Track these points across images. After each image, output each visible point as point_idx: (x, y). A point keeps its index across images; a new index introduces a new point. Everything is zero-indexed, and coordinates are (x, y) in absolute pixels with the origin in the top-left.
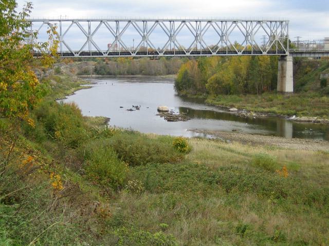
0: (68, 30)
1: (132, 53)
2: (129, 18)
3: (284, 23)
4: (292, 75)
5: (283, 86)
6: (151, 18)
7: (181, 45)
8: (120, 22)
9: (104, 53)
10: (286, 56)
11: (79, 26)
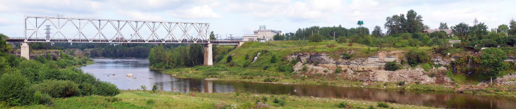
0: (84, 26)
1: (128, 41)
2: (108, 19)
3: (207, 25)
4: (212, 56)
5: (207, 62)
6: (174, 21)
7: (66, 38)
8: (138, 22)
9: (110, 40)
10: (208, 44)
11: (112, 24)
